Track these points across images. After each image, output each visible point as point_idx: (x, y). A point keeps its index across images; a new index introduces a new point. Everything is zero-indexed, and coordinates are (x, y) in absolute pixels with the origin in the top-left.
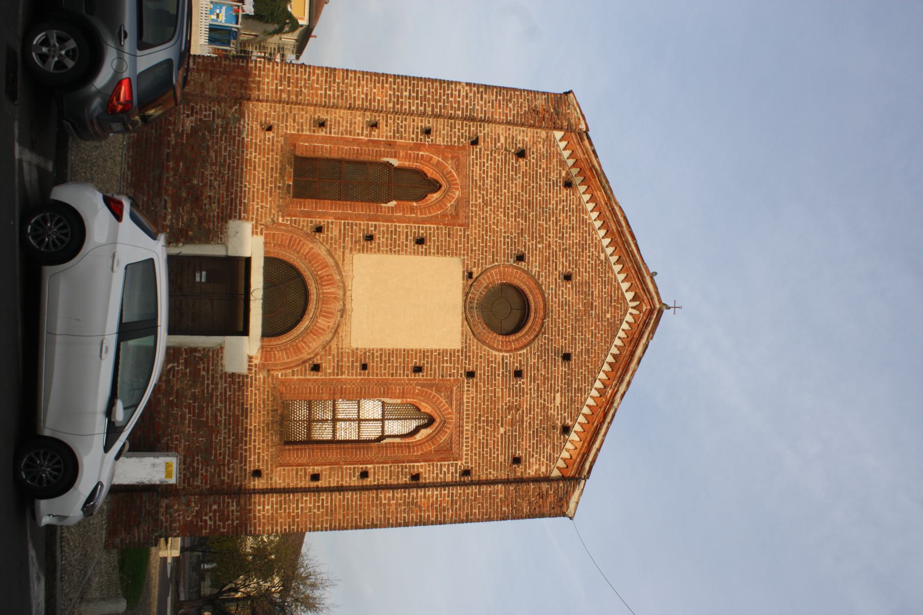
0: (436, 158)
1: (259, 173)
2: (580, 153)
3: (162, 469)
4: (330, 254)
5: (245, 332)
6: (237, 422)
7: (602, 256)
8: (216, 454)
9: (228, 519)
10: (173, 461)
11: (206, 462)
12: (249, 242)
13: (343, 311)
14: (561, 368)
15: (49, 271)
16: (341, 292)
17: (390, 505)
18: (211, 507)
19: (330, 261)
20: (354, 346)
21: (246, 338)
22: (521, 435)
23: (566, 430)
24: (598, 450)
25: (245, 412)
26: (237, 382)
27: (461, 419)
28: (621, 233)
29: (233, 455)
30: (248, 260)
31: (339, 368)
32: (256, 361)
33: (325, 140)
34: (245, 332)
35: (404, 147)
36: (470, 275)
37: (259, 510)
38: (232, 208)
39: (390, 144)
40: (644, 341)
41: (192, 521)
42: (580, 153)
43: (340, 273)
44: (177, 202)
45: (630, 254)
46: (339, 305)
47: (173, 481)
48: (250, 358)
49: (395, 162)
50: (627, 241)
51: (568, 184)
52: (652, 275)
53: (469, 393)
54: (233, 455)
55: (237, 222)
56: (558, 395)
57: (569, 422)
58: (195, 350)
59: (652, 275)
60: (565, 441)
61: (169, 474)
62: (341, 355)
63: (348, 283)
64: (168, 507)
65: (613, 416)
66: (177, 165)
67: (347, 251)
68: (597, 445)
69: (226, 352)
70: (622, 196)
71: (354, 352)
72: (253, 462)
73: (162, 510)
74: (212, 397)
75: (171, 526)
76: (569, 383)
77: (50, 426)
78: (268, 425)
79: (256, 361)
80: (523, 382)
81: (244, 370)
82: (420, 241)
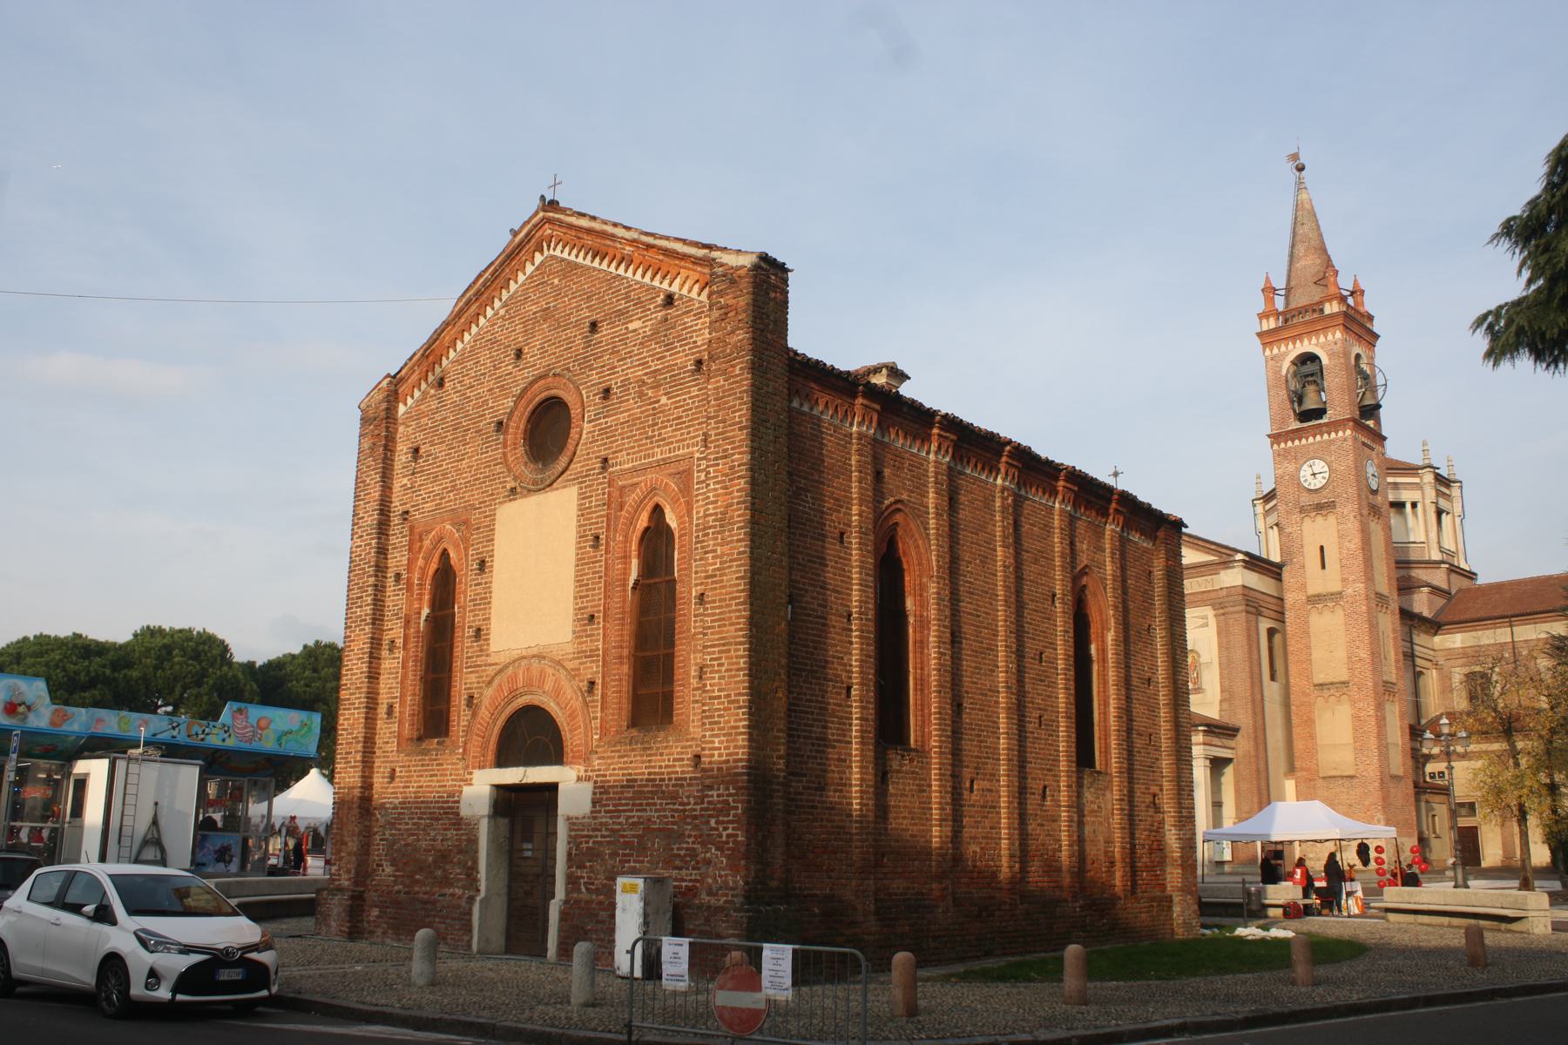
0: (420, 562)
1: (424, 781)
2: (415, 377)
3: (627, 897)
4: (490, 683)
5: (552, 788)
6: (640, 794)
7: (502, 312)
8: (673, 823)
9: (727, 802)
10: (621, 881)
11: (681, 836)
12: (479, 786)
13: (540, 657)
14: (605, 330)
15: (16, 973)
16: (523, 663)
17: (723, 555)
18: (712, 829)
19: (496, 682)
20: (570, 637)
21: (560, 787)
22: (670, 368)
23: (670, 300)
24: (684, 241)
25: (631, 783)
26: (602, 794)
27: (650, 466)
28: (479, 294)
29: (674, 797)
30: (499, 788)
31: (592, 654)
32: (582, 773)
33: (402, 703)
34: (552, 788)
35: (410, 605)
36: (513, 490)
37: (720, 755)
38: (447, 812)
39: (407, 622)
40: (573, 220)
41: (728, 857)
42: (415, 377)
43: (506, 667)
44: (446, 881)
45: (496, 275)
46: (535, 663)
47: (640, 882)
48: (579, 779)
49: (426, 611)
50: (484, 284)
51: (441, 383)
52: (515, 233)
53: (623, 462)
54: (674, 797)
55: (462, 805)
56: (631, 326)
57: (660, 300)
58: (569, 854)
59: (515, 233)
60: (681, 297)
61: (633, 888)
62: (581, 654)
63: (515, 654)
64: (710, 894)
65: (647, 234)
66: (417, 881)
67: (490, 660)
68: (679, 247)
69: (573, 813)
70: (443, 309)
71: (577, 635)
72: (683, 768)
73: (713, 901)
74: (612, 830)
75: (733, 889)
76: (620, 313)
77: (84, 976)
78: (645, 749)
79: (582, 773)
80: (615, 383)
81: (589, 786)
82: (482, 563)
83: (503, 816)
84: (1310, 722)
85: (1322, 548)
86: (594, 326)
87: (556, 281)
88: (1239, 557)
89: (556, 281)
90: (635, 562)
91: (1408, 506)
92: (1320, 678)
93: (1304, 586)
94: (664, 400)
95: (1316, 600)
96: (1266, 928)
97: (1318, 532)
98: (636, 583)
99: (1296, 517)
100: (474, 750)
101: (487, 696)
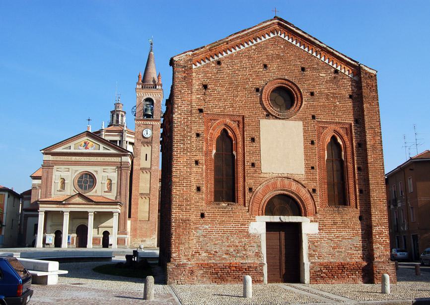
14: (308, 72)
23: (336, 71)
31: (314, 180)
49: (214, 151)
56: (321, 75)
63: (275, 175)
67: (262, 175)
80: (316, 91)
83: (95, 228)
84: (137, 204)
85: (146, 155)
86: (303, 69)
87: (282, 46)
88: (129, 153)
89: (282, 46)
90: (326, 152)
91: (118, 142)
92: (142, 192)
93: (139, 165)
94: (338, 103)
95: (143, 169)
96: (262, 265)
97: (145, 150)
98: (327, 160)
99: (140, 144)
100: (255, 208)
101: (259, 189)
